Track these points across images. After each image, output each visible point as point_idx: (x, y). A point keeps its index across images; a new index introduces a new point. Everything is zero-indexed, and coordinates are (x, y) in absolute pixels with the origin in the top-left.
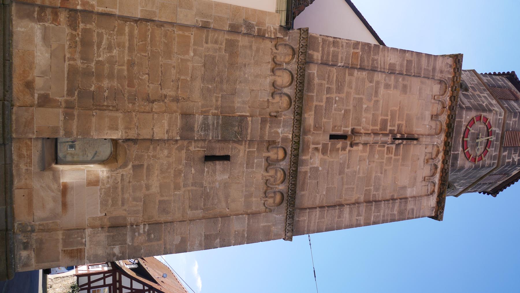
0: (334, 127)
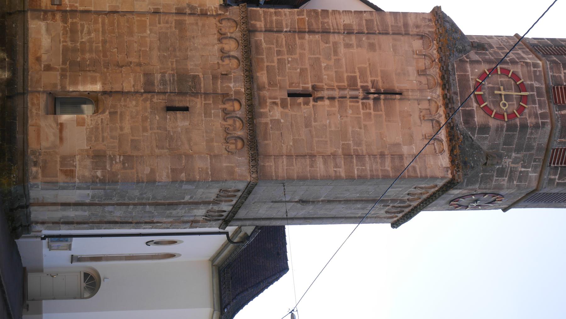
0: (291, 84)
